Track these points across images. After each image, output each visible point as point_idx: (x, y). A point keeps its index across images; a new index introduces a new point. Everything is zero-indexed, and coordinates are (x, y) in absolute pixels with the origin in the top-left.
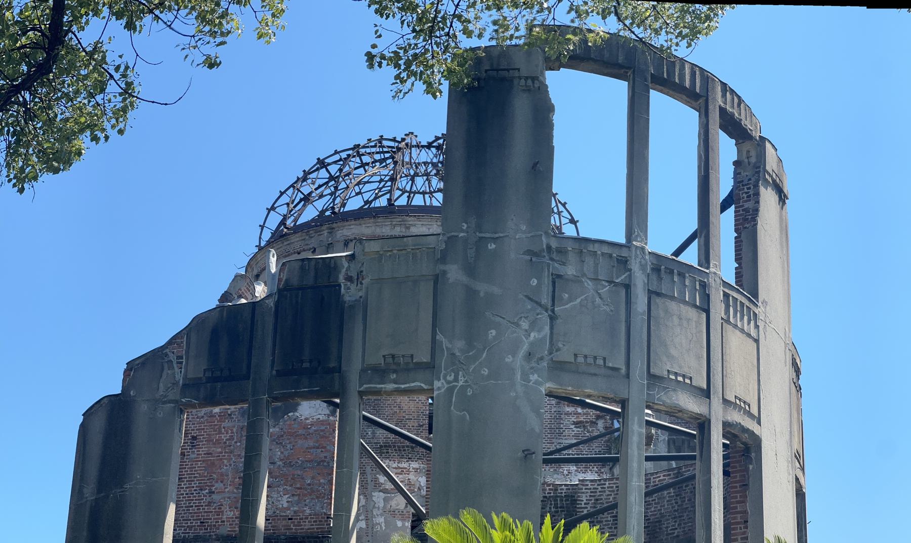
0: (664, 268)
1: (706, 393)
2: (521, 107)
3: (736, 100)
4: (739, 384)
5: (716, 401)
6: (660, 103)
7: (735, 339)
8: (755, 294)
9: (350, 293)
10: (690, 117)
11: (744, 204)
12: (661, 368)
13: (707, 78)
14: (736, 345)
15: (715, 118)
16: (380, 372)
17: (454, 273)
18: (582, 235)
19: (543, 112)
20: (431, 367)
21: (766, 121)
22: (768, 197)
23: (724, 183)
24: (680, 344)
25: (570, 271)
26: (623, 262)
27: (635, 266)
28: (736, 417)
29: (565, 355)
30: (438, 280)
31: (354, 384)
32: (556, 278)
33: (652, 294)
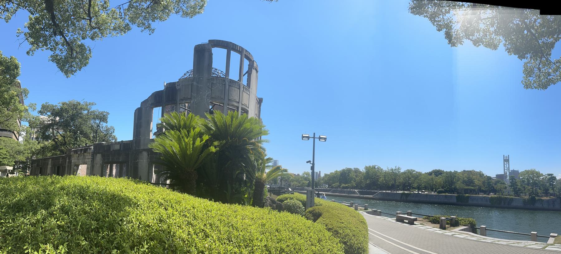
0: (232, 81)
1: (239, 103)
2: (207, 54)
3: (246, 63)
4: (245, 101)
5: (240, 104)
6: (233, 53)
7: (245, 94)
8: (250, 87)
9: (178, 88)
10: (239, 56)
11: (249, 73)
12: (230, 98)
13: (242, 49)
14: (245, 96)
15: (244, 56)
16: (182, 100)
17: (195, 83)
18: (225, 51)
19: (211, 55)
20: (191, 99)
21: (255, 58)
22: (254, 71)
23: (246, 69)
24: (234, 94)
25: (215, 82)
26: (224, 81)
27: (226, 81)
28: (244, 107)
29: (213, 96)
30: (192, 85)
31: (178, 102)
32: (212, 83)
33: (229, 86)
